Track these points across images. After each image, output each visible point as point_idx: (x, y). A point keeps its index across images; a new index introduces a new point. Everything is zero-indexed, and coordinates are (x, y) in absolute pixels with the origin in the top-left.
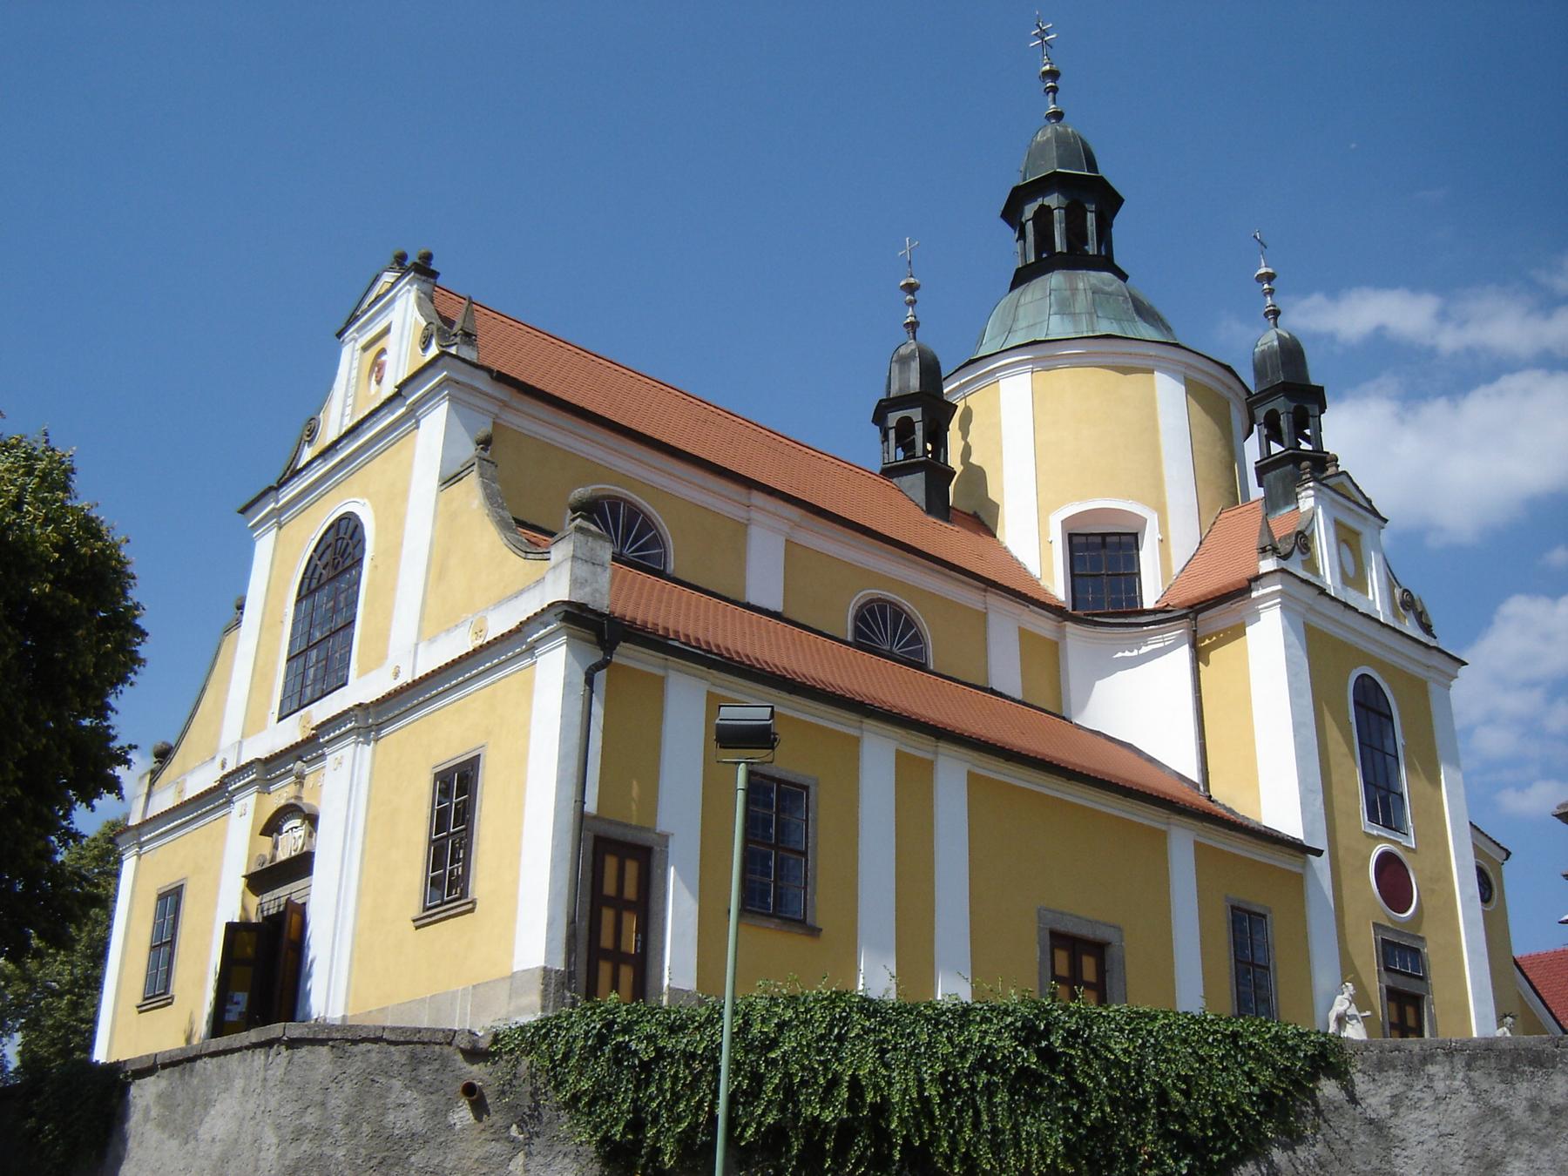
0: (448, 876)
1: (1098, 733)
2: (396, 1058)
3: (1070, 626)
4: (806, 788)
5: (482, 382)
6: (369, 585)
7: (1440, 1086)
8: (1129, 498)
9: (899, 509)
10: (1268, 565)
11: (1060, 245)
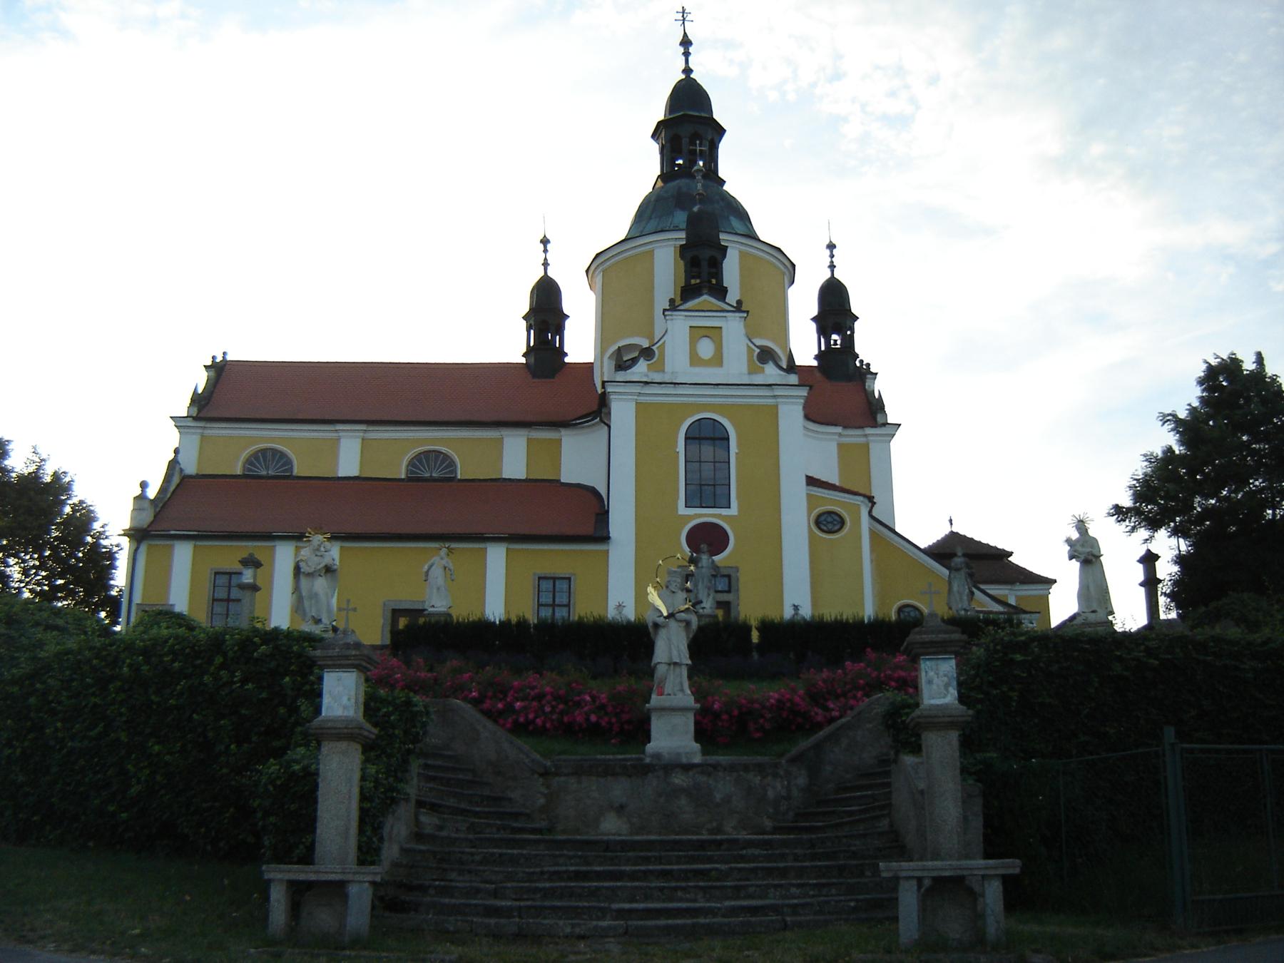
8: (615, 343)
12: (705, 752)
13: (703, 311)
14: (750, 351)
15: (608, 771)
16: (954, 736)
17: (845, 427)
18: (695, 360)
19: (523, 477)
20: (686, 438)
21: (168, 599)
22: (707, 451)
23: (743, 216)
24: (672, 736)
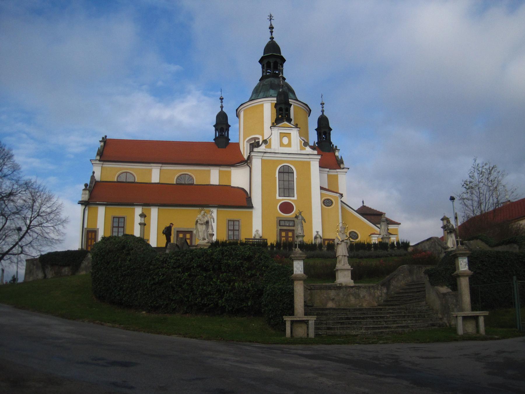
12: (355, 283)
13: (285, 127)
14: (301, 142)
15: (330, 288)
16: (467, 278)
17: (330, 169)
18: (282, 145)
19: (218, 184)
20: (279, 172)
21: (96, 226)
22: (286, 176)
23: (293, 92)
24: (344, 278)
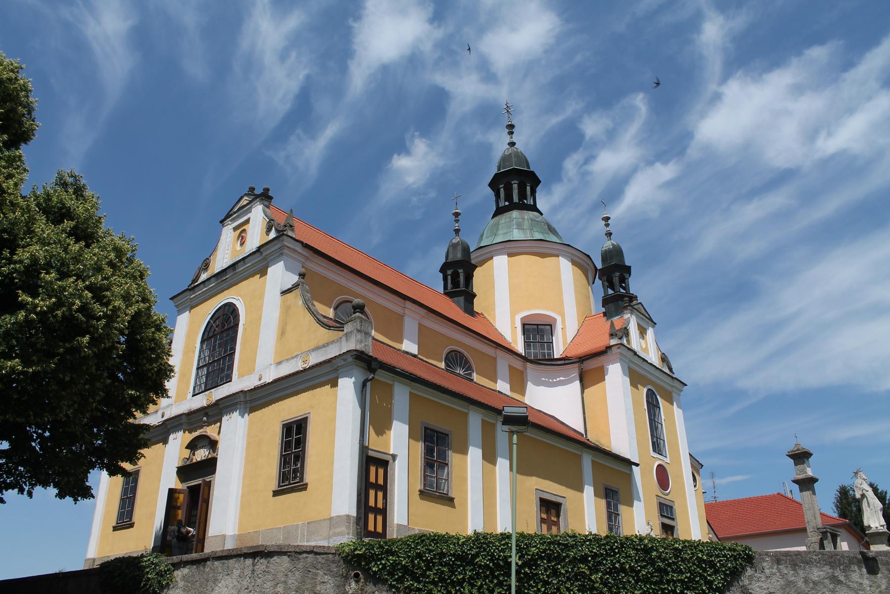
0: (292, 473)
1: (540, 411)
2: (320, 560)
3: (529, 365)
4: (447, 435)
5: (299, 248)
6: (243, 335)
7: (767, 571)
9: (452, 309)
10: (613, 342)
11: (516, 199)
